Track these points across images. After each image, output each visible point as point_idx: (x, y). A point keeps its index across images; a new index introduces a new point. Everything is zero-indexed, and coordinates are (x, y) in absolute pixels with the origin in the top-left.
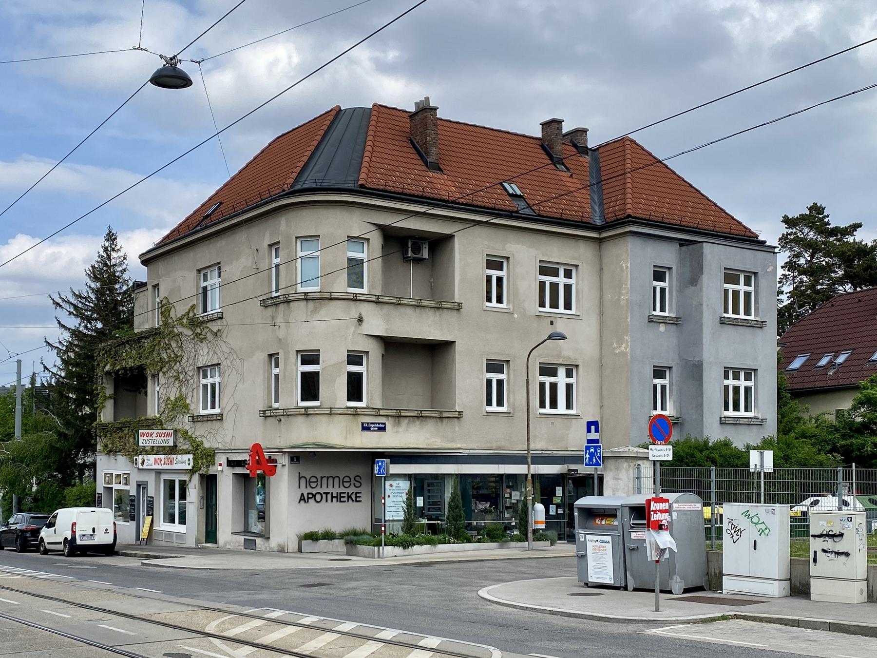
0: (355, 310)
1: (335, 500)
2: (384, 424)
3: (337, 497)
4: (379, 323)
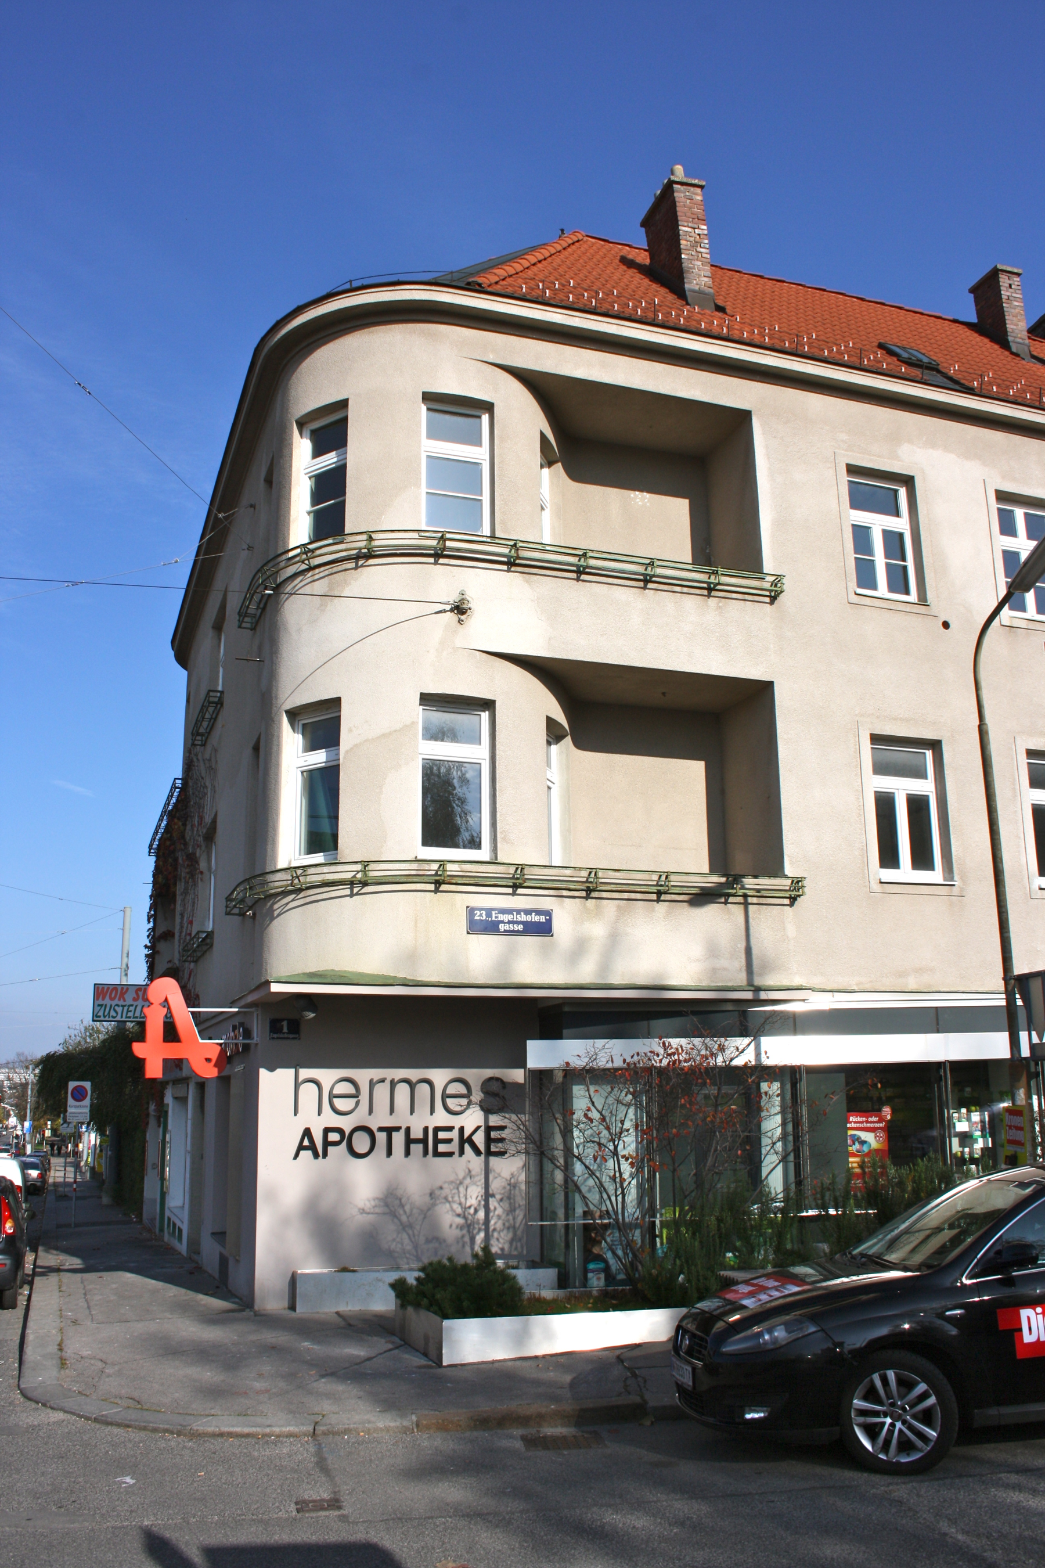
0: (447, 581)
1: (417, 1149)
2: (548, 913)
3: (424, 1141)
4: (523, 616)
